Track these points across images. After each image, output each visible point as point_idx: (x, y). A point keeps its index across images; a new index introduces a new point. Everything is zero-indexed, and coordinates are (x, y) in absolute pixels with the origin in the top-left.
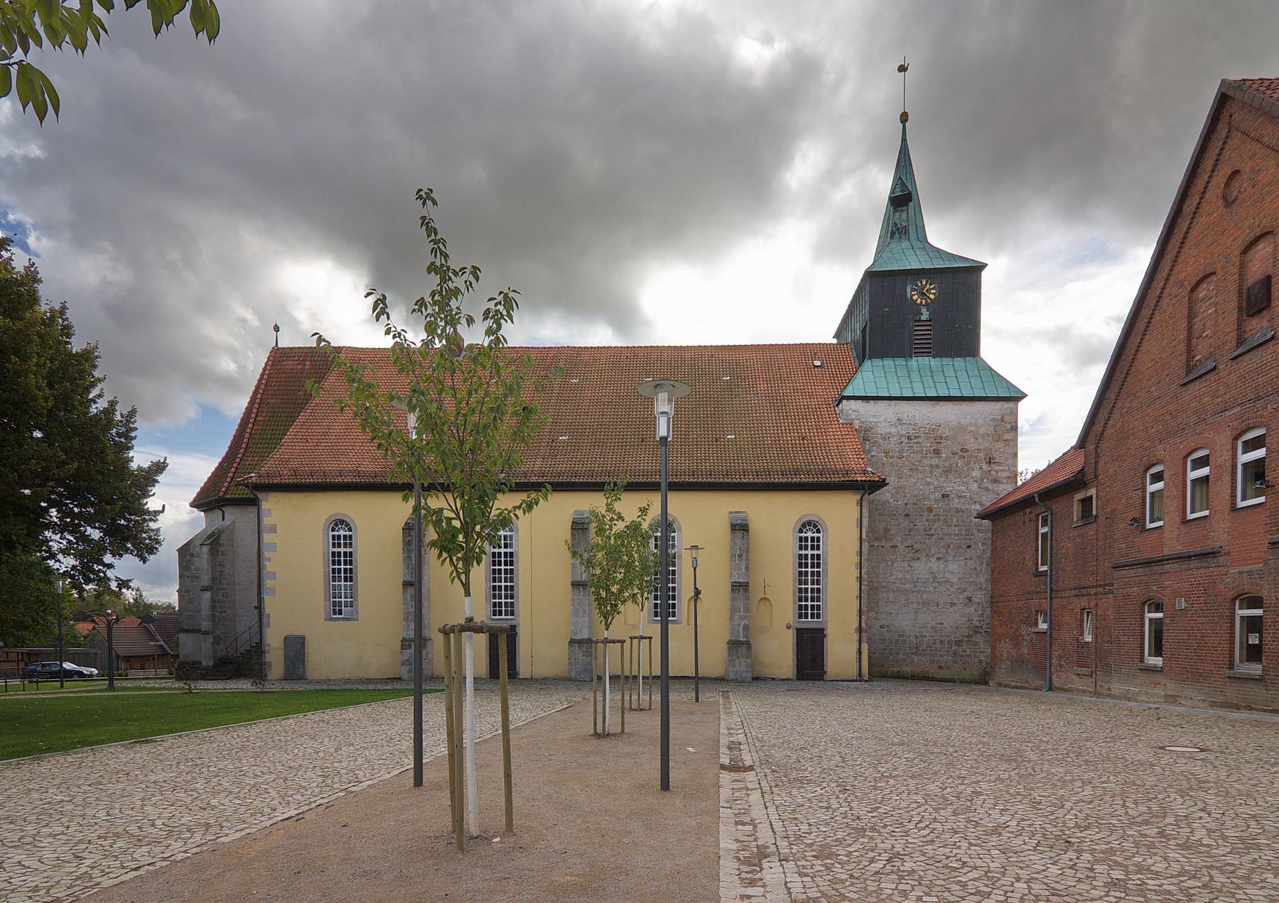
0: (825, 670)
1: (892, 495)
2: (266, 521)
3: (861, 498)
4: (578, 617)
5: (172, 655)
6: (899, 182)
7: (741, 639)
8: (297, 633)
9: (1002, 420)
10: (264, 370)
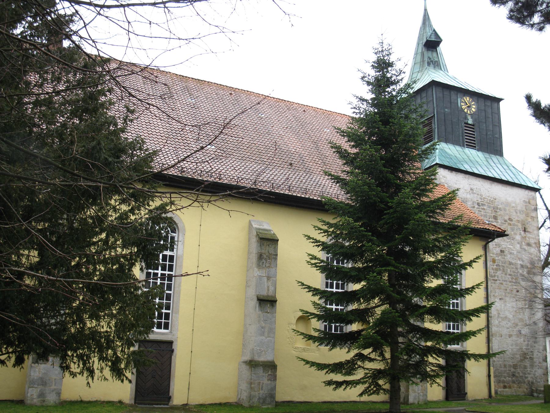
0: (466, 392)
9: (529, 203)
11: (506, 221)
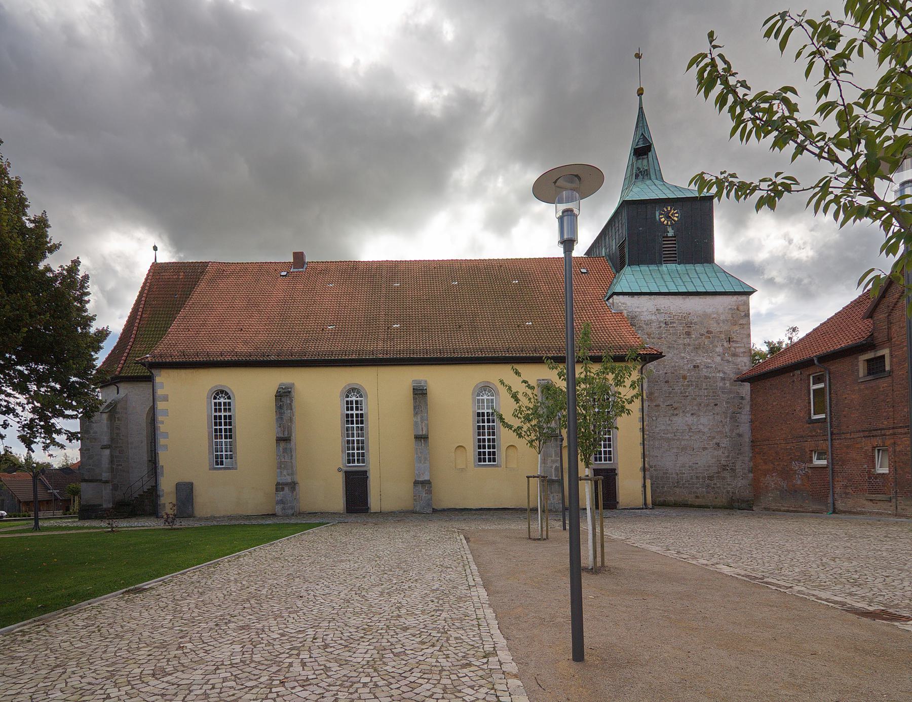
0: (617, 501)
1: (655, 366)
2: (160, 392)
3: (642, 367)
5: (61, 500)
6: (641, 137)
7: (554, 478)
8: (188, 481)
9: (738, 309)
10: (148, 275)
11: (702, 335)
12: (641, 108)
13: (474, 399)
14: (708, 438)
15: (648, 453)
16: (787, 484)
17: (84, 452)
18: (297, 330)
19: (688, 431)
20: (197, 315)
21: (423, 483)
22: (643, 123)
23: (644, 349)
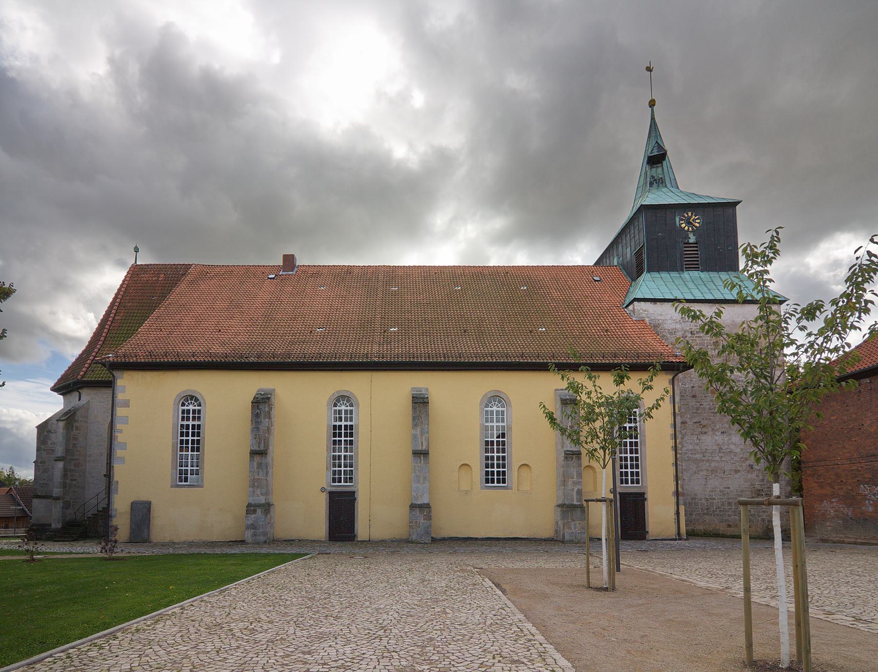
0: (647, 530)
2: (120, 396)
3: (673, 378)
4: (419, 483)
6: (656, 145)
7: (575, 503)
10: (124, 281)
12: (653, 119)
13: (482, 409)
14: (740, 459)
15: (681, 475)
16: (853, 511)
17: (39, 464)
18: (282, 331)
19: (718, 451)
20: (172, 315)
21: (421, 507)
22: (656, 133)
23: (676, 357)
